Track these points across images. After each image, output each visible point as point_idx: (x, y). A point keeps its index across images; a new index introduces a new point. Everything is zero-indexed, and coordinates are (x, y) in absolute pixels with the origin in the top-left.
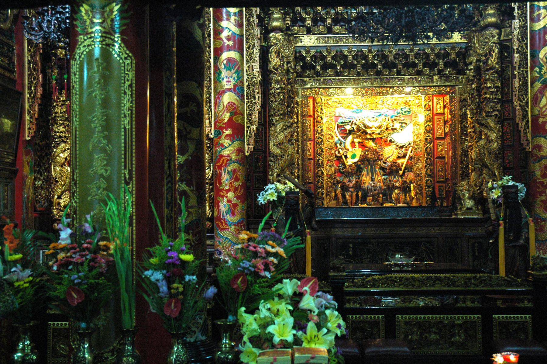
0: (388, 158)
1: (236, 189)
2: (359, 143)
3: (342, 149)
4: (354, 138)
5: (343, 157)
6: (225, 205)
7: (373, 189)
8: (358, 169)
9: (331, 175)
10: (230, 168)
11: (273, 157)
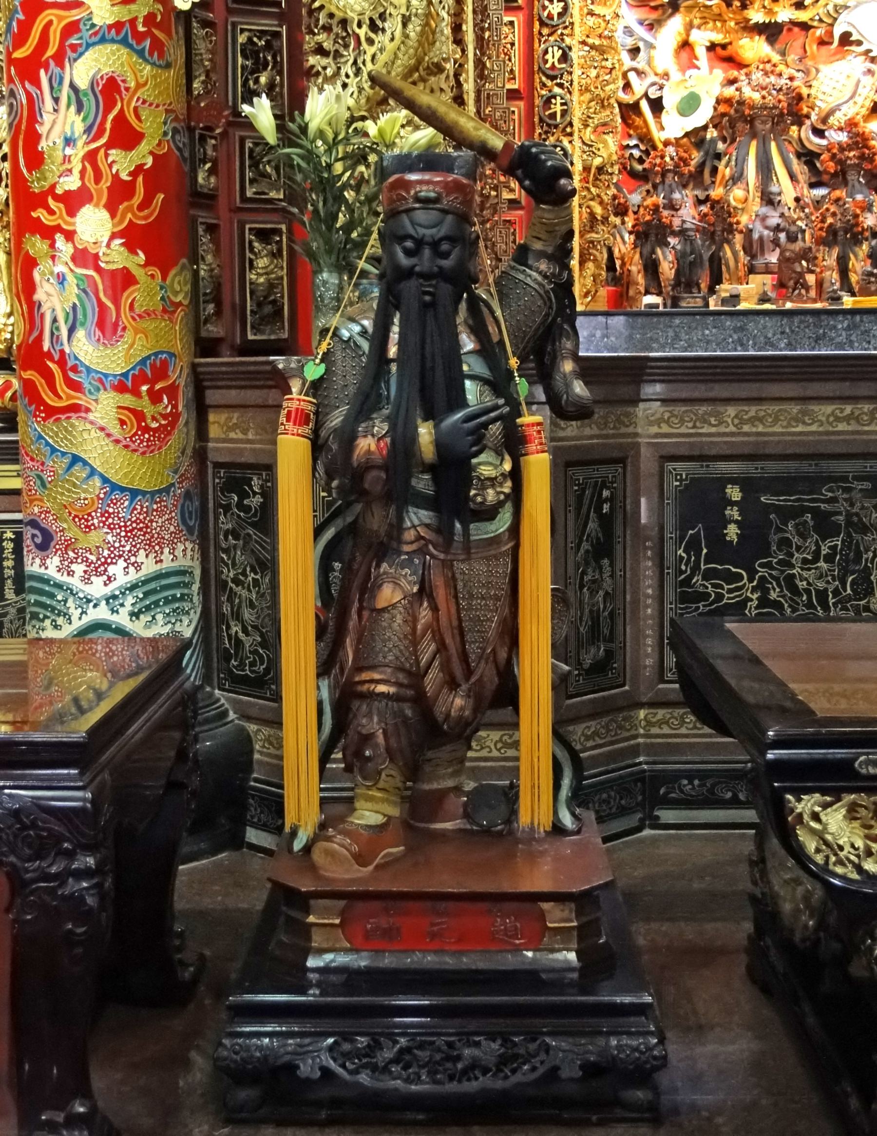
0: (831, 112)
1: (119, 192)
2: (712, 47)
3: (639, 73)
4: (689, 27)
5: (644, 106)
6: (61, 279)
7: (782, 236)
8: (700, 163)
9: (600, 170)
10: (84, 70)
11: (327, 29)
